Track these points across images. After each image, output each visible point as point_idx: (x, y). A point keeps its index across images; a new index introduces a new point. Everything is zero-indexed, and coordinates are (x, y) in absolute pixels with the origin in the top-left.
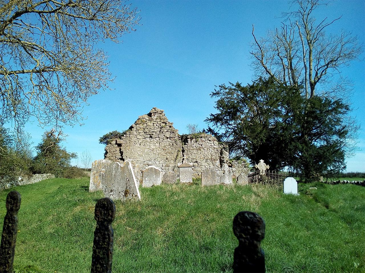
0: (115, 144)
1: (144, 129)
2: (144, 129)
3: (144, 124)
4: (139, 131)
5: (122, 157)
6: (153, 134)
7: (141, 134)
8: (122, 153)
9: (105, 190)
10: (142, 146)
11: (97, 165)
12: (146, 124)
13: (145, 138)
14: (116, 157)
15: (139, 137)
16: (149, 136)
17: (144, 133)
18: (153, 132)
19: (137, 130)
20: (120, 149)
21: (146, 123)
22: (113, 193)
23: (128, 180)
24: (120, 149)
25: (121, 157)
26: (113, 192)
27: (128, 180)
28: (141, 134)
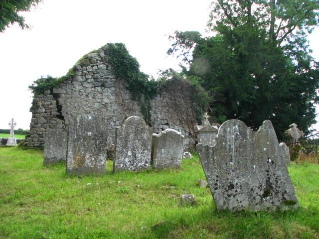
0: (50, 94)
1: (94, 73)
2: (94, 73)
3: (94, 66)
4: (87, 77)
5: (61, 113)
6: (106, 82)
7: (89, 81)
8: (59, 108)
9: (216, 184)
10: (90, 98)
11: (78, 124)
12: (97, 66)
13: (95, 87)
14: (51, 114)
15: (85, 84)
16: (100, 84)
17: (94, 79)
18: (107, 78)
19: (84, 74)
20: (58, 103)
21: (97, 64)
22: (236, 191)
23: (272, 162)
24: (58, 103)
25: (59, 114)
26: (235, 189)
27: (270, 161)
28: (89, 81)
